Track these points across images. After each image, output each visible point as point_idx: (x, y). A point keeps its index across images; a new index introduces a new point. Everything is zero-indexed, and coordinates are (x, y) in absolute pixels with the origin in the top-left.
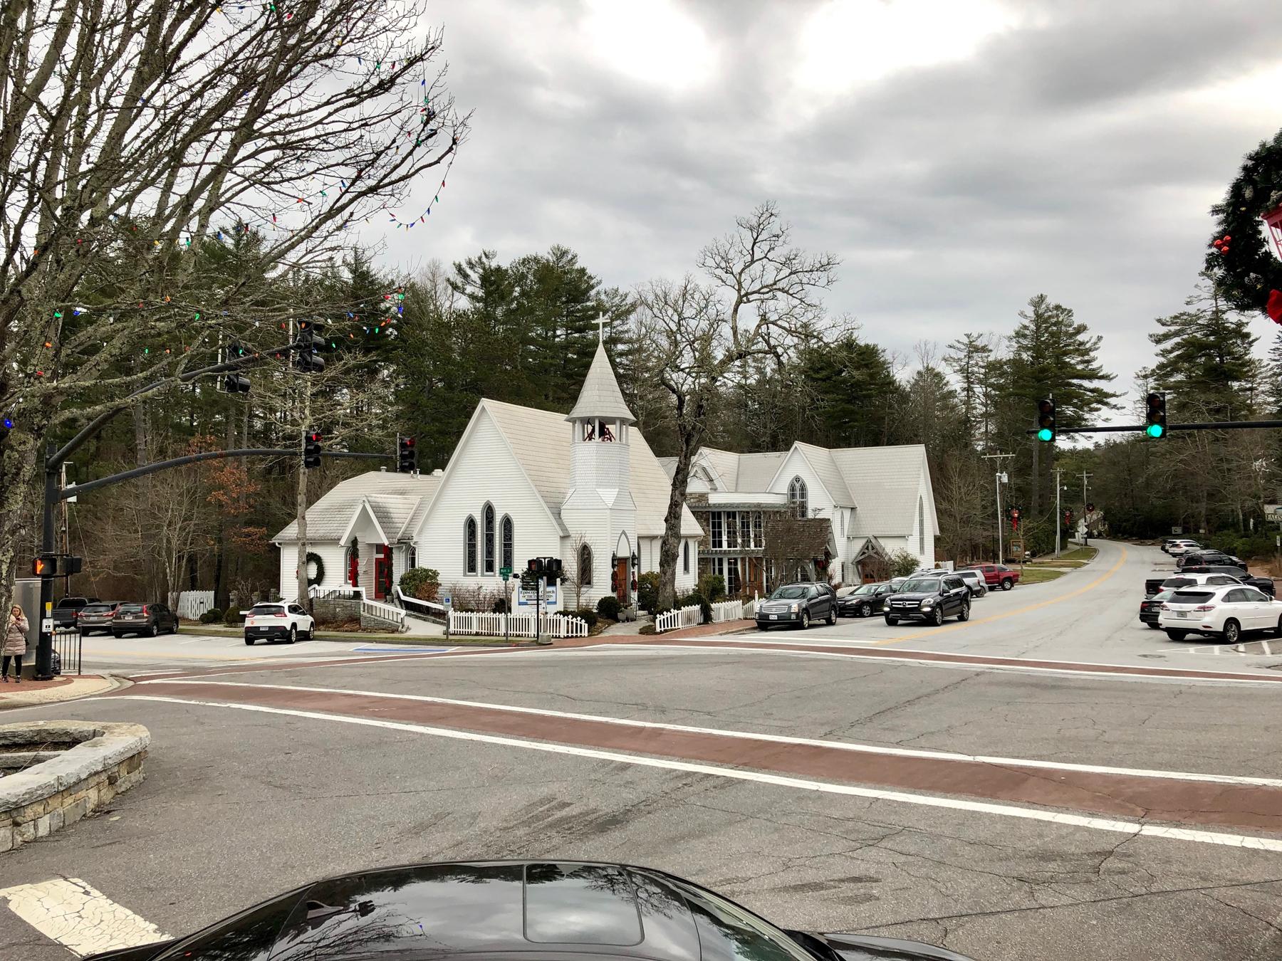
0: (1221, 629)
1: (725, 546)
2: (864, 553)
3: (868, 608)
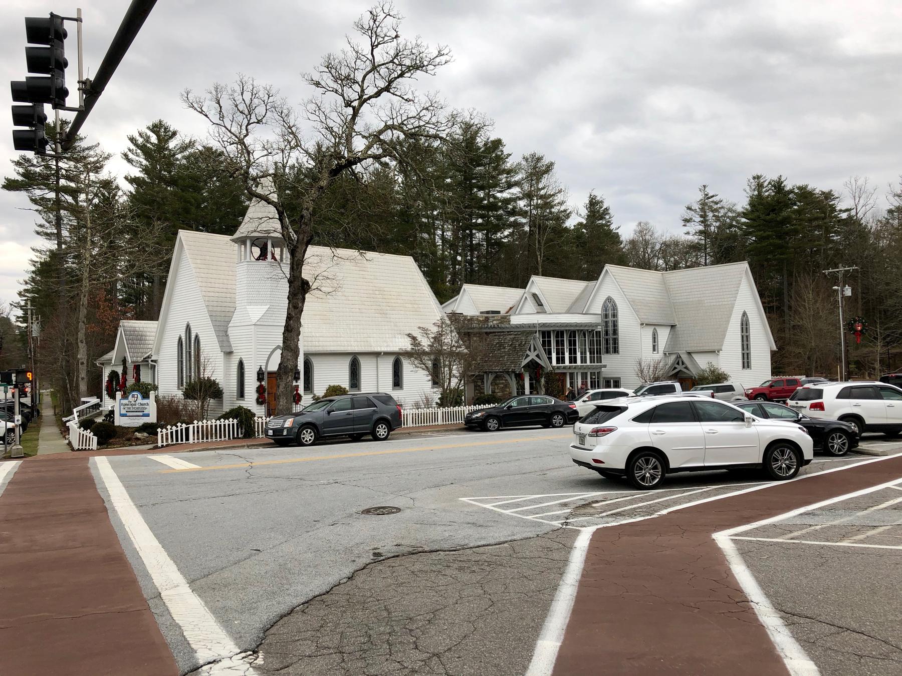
0: (622, 466)
1: (567, 363)
2: (675, 368)
3: (495, 421)
